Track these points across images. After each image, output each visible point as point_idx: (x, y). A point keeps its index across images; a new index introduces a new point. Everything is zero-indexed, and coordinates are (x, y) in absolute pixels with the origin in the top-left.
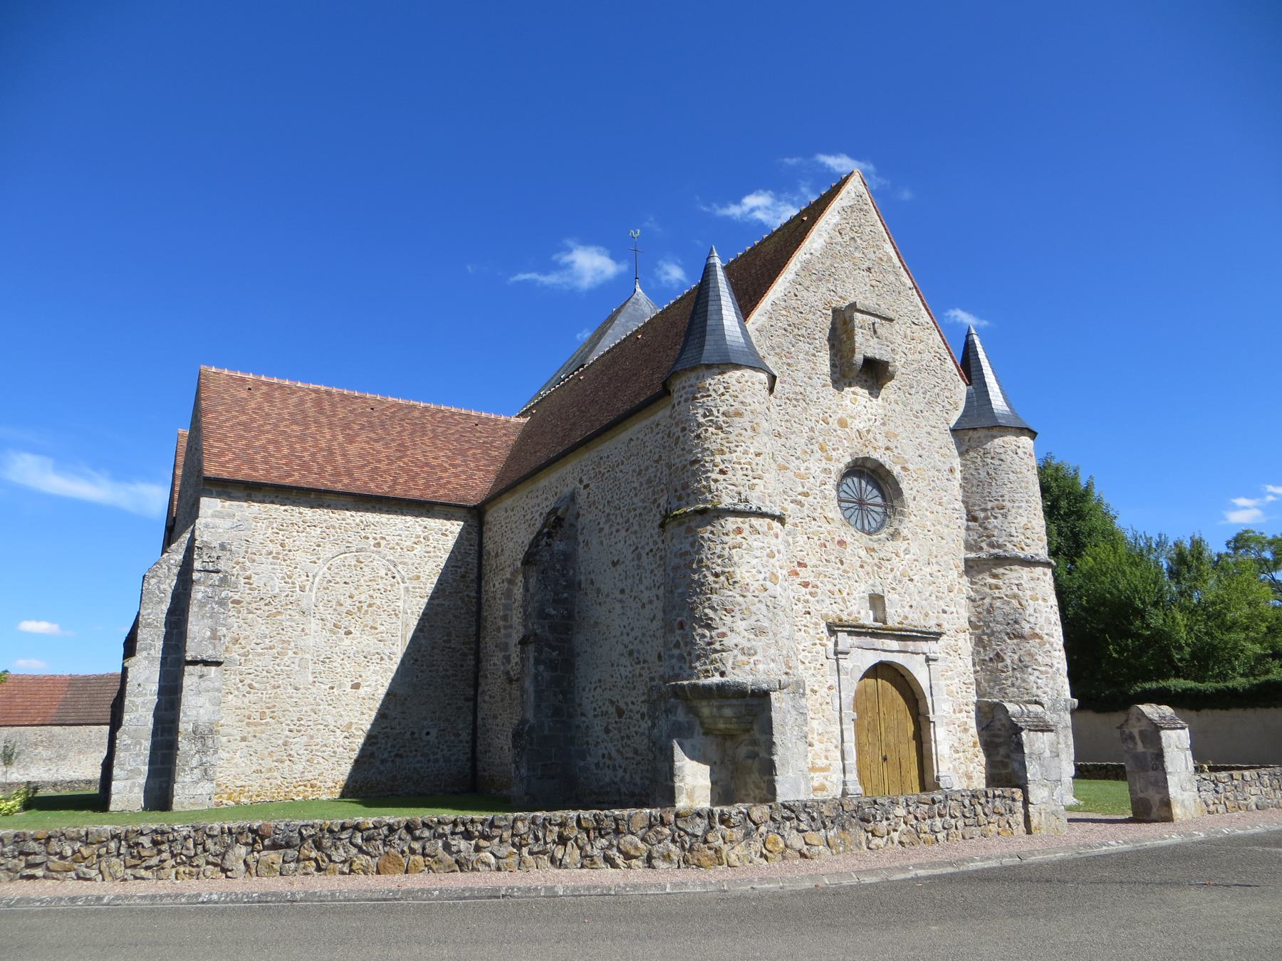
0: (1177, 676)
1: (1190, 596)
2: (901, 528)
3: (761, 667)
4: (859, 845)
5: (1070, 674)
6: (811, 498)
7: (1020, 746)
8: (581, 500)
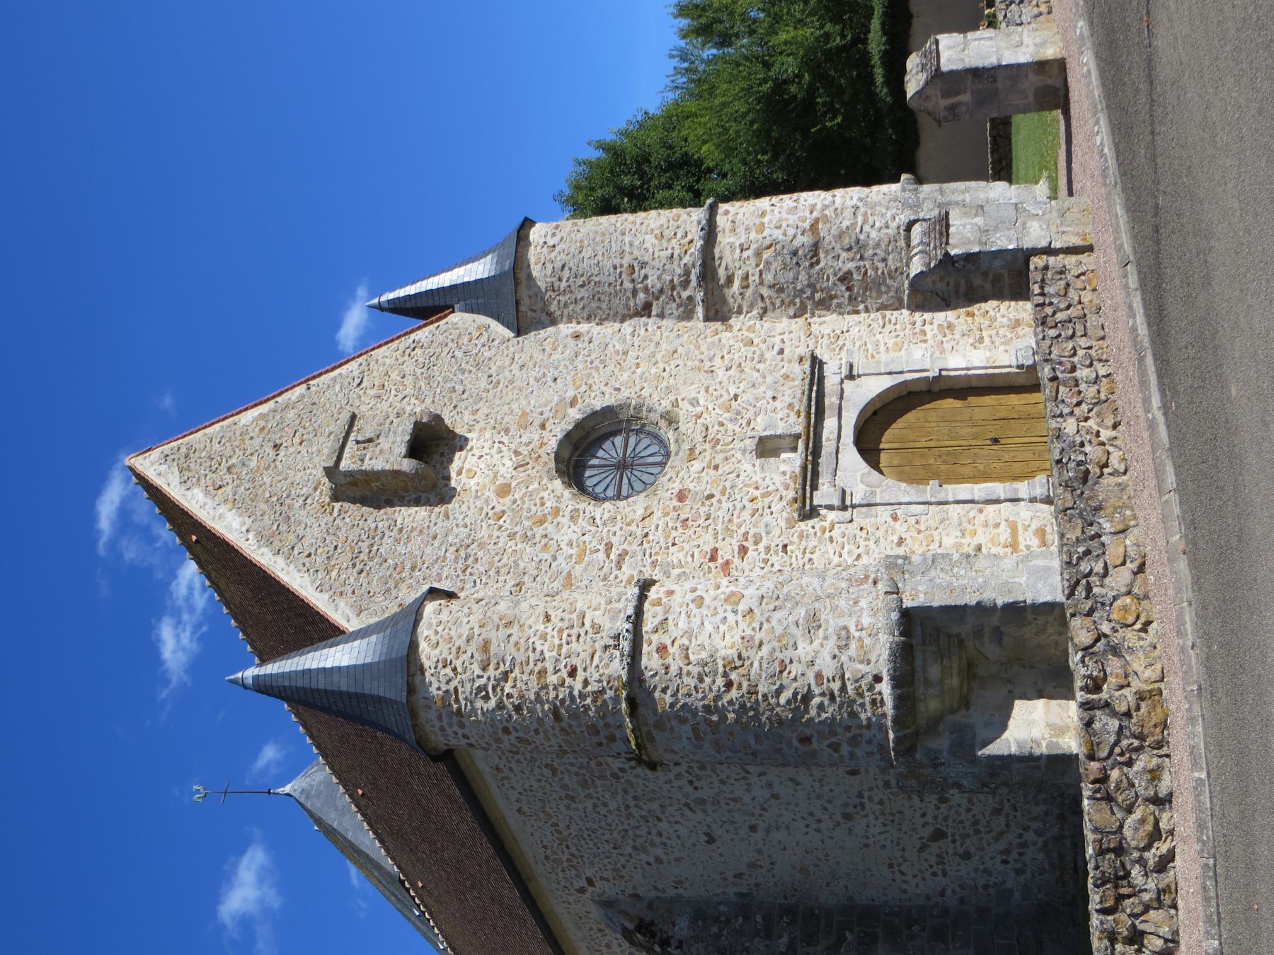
0: (865, 41)
1: (755, 21)
2: (660, 410)
3: (866, 621)
4: (1122, 487)
5: (868, 183)
6: (614, 540)
7: (969, 258)
8: (612, 891)
